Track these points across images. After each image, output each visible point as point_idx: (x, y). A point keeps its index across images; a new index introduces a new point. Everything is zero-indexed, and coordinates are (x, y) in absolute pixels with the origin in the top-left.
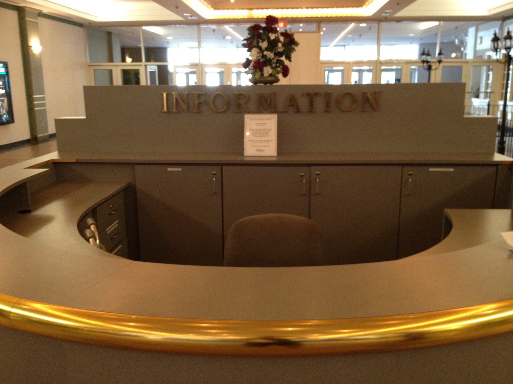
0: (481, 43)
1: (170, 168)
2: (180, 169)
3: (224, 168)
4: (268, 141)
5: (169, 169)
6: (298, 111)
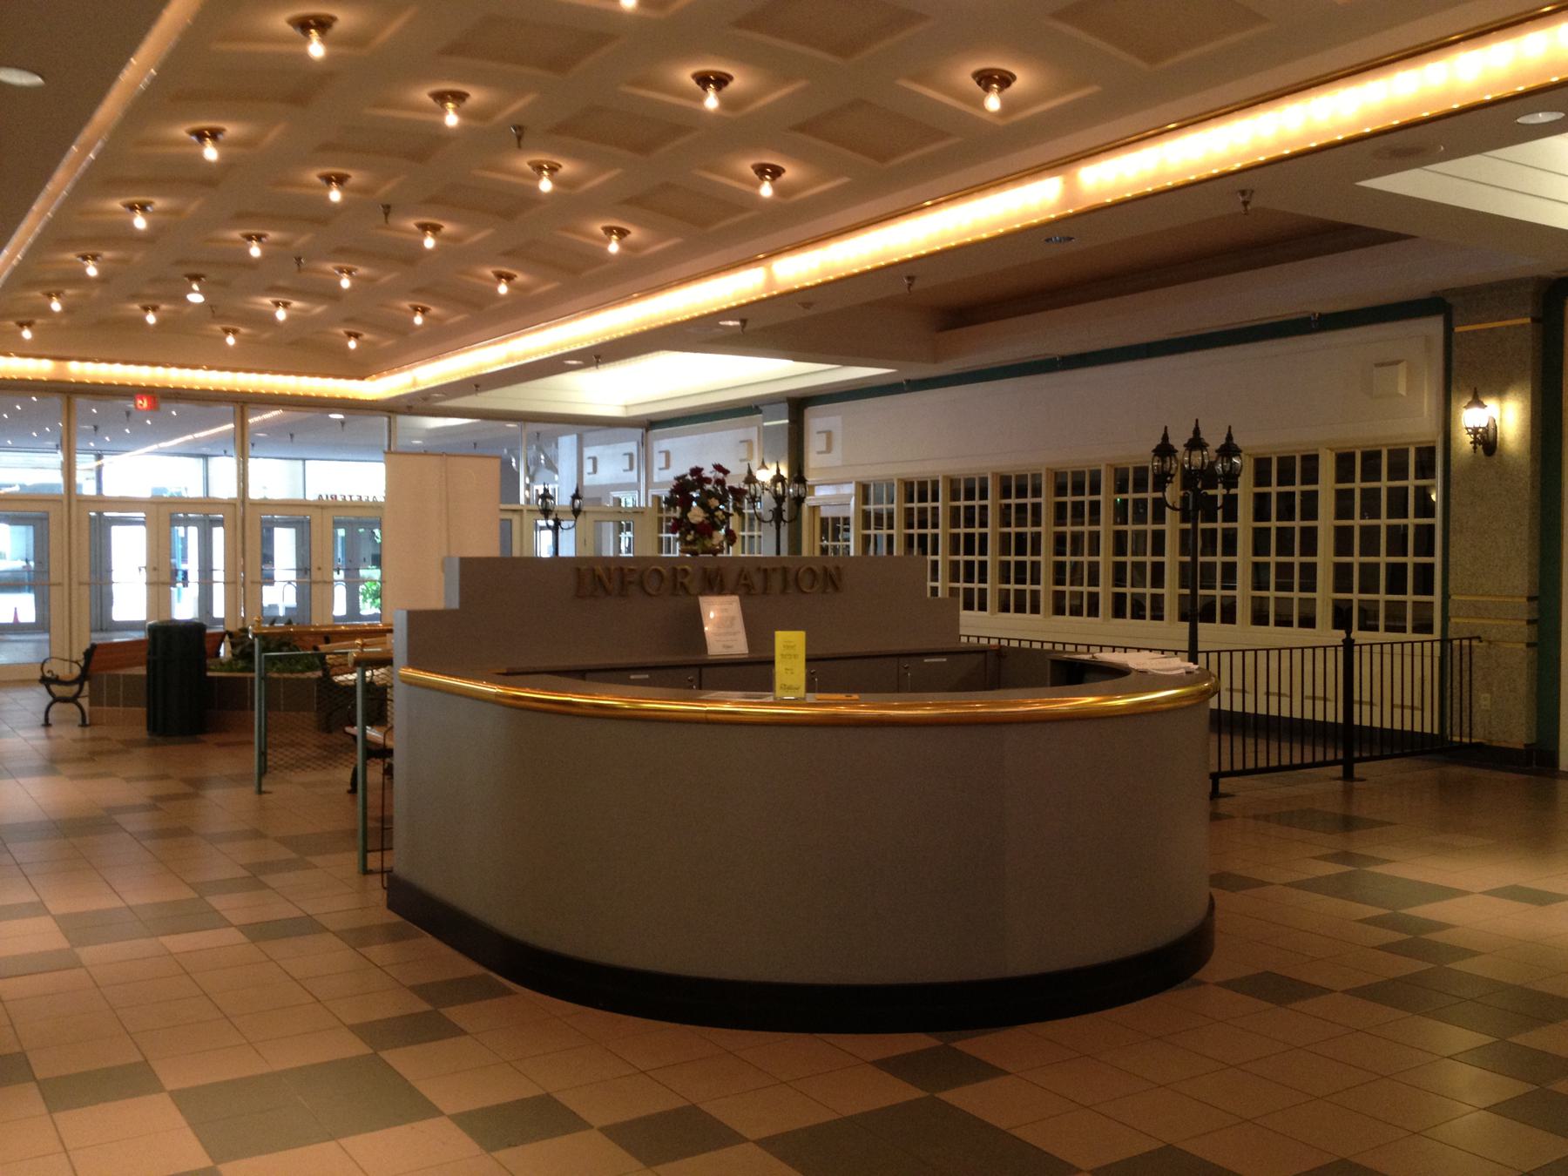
0: (595, 471)
1: (634, 674)
2: (647, 676)
3: (705, 670)
4: (735, 634)
5: (926, 661)
6: (607, 593)
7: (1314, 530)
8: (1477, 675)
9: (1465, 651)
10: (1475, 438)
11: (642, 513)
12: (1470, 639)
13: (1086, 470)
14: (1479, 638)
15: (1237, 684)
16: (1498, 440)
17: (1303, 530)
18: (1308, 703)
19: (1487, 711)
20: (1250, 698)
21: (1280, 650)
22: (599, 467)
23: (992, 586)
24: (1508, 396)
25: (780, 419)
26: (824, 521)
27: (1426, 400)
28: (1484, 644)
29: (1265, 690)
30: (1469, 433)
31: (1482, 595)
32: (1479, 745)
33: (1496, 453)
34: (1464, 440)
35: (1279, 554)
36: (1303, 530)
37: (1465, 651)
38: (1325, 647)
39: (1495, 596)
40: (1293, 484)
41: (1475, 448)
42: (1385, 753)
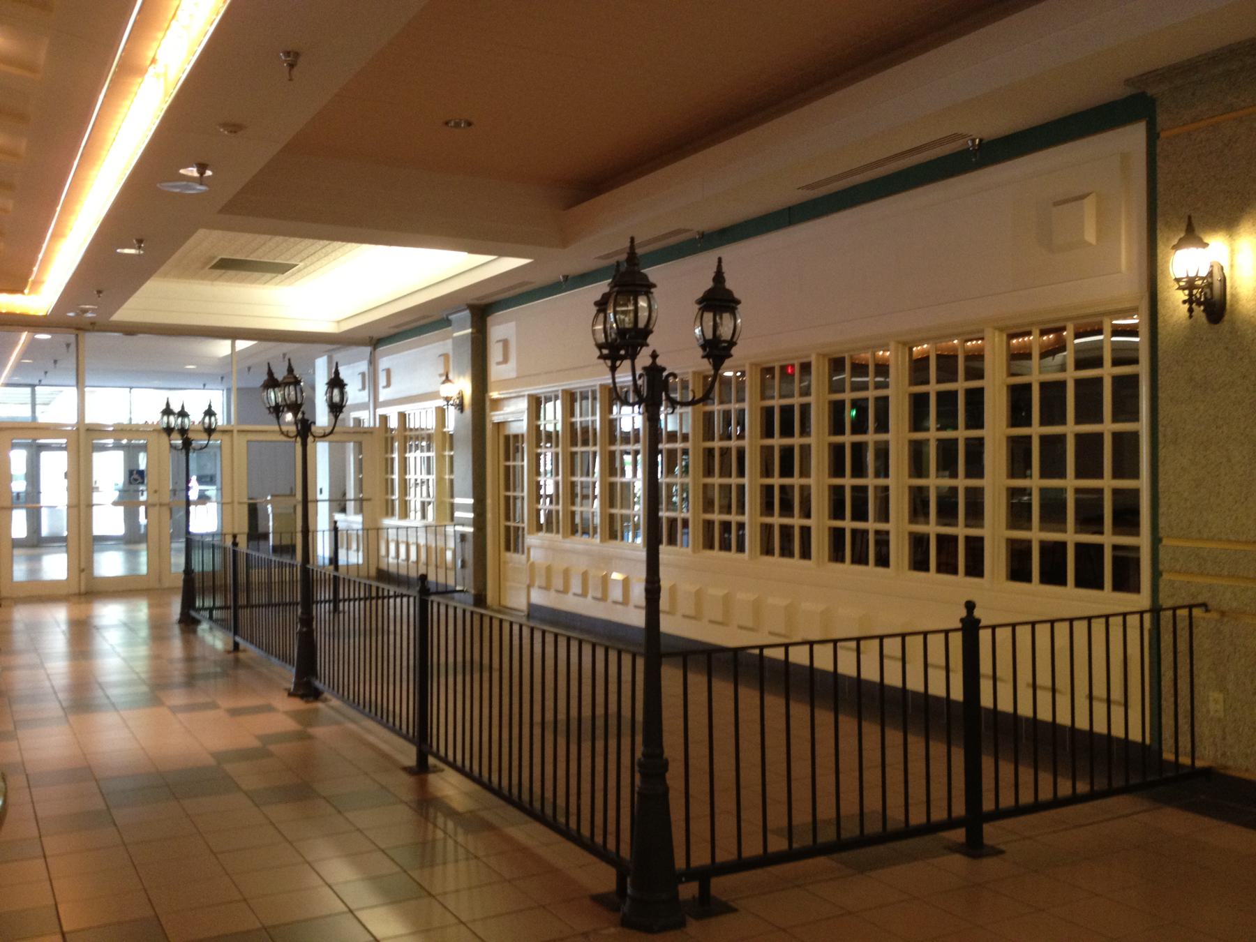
7: (980, 442)
8: (1202, 665)
9: (1183, 625)
10: (1191, 295)
11: (371, 433)
12: (1190, 607)
13: (578, 391)
14: (1204, 606)
15: (1044, 679)
16: (1228, 297)
17: (1044, 439)
18: (1100, 708)
19: (1219, 720)
20: (1063, 702)
21: (1052, 622)
22: (393, 380)
23: (751, 518)
24: (1242, 230)
25: (465, 329)
26: (507, 438)
27: (1123, 245)
28: (1214, 615)
29: (1030, 680)
30: (1181, 288)
31: (1208, 539)
32: (1207, 772)
33: (1226, 317)
34: (1175, 301)
35: (1079, 475)
36: (1044, 439)
37: (1183, 625)
38: (1089, 619)
39: (1229, 541)
40: (955, 380)
41: (1191, 310)
42: (1132, 782)
